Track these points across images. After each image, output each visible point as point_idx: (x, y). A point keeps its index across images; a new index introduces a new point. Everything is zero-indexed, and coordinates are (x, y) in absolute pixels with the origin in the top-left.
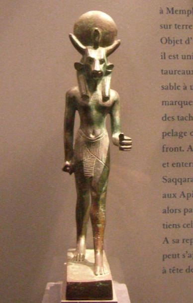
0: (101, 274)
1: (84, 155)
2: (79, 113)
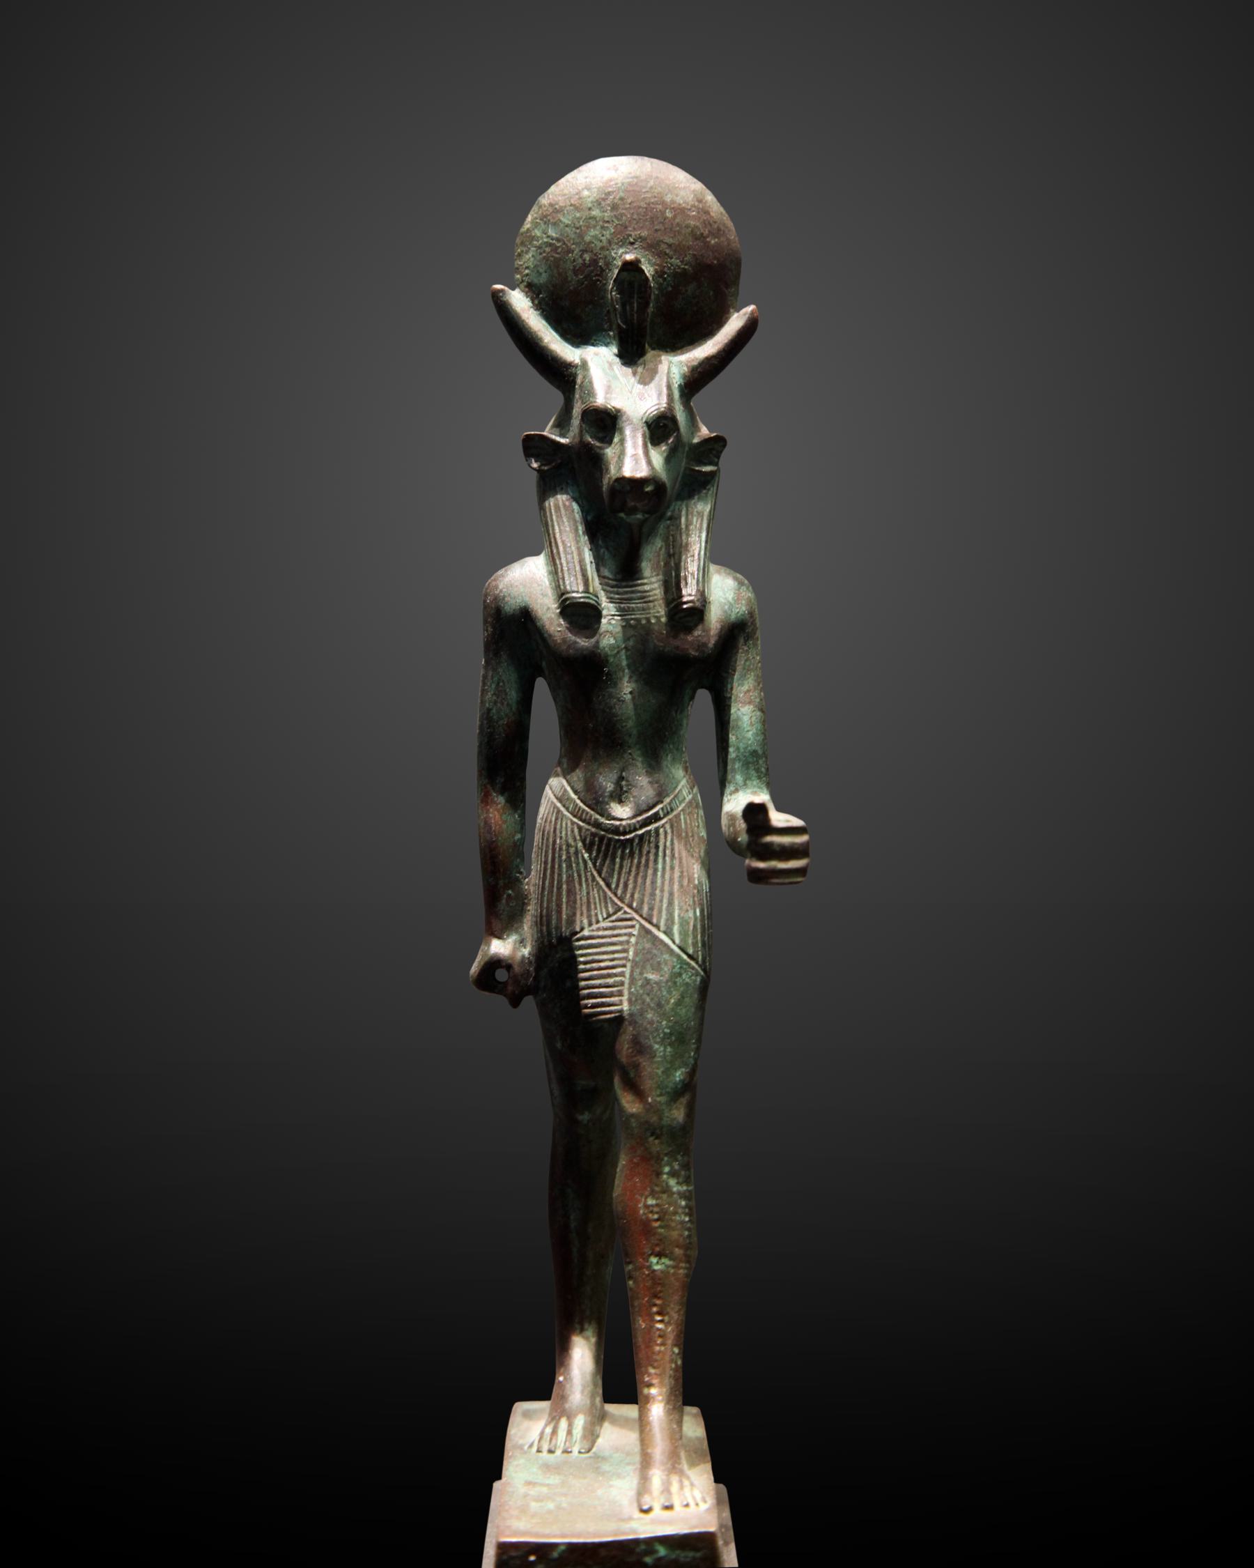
0: (669, 1508)
1: (581, 908)
2: (554, 689)
